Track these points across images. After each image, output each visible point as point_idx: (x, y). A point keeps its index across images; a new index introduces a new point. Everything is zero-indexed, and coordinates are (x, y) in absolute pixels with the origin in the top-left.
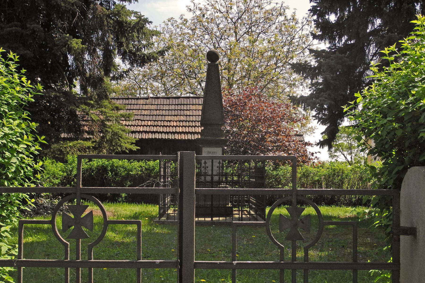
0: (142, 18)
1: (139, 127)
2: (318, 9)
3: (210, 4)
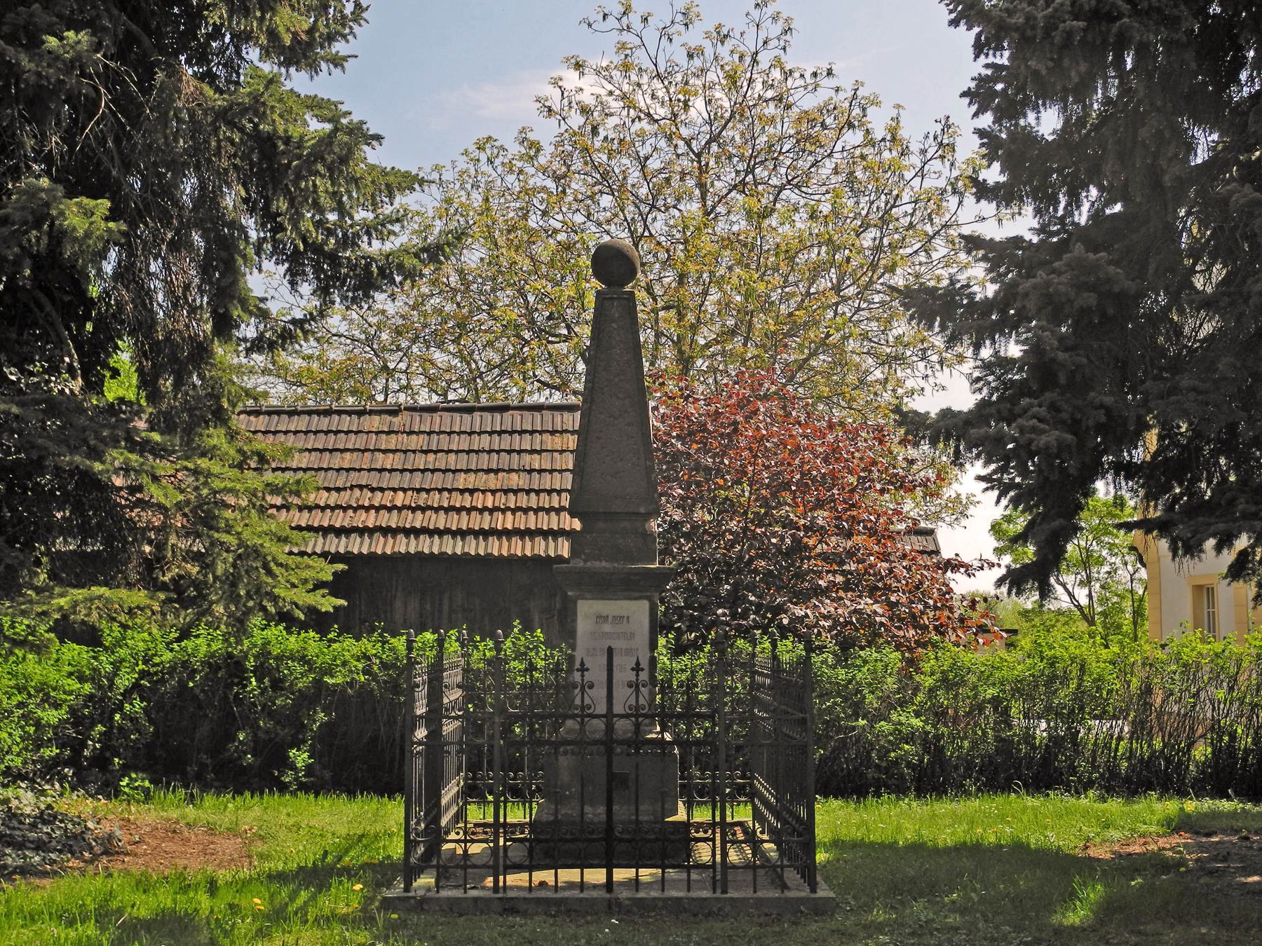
0: (344, 121)
1: (364, 515)
2: (999, 87)
3: (617, 92)
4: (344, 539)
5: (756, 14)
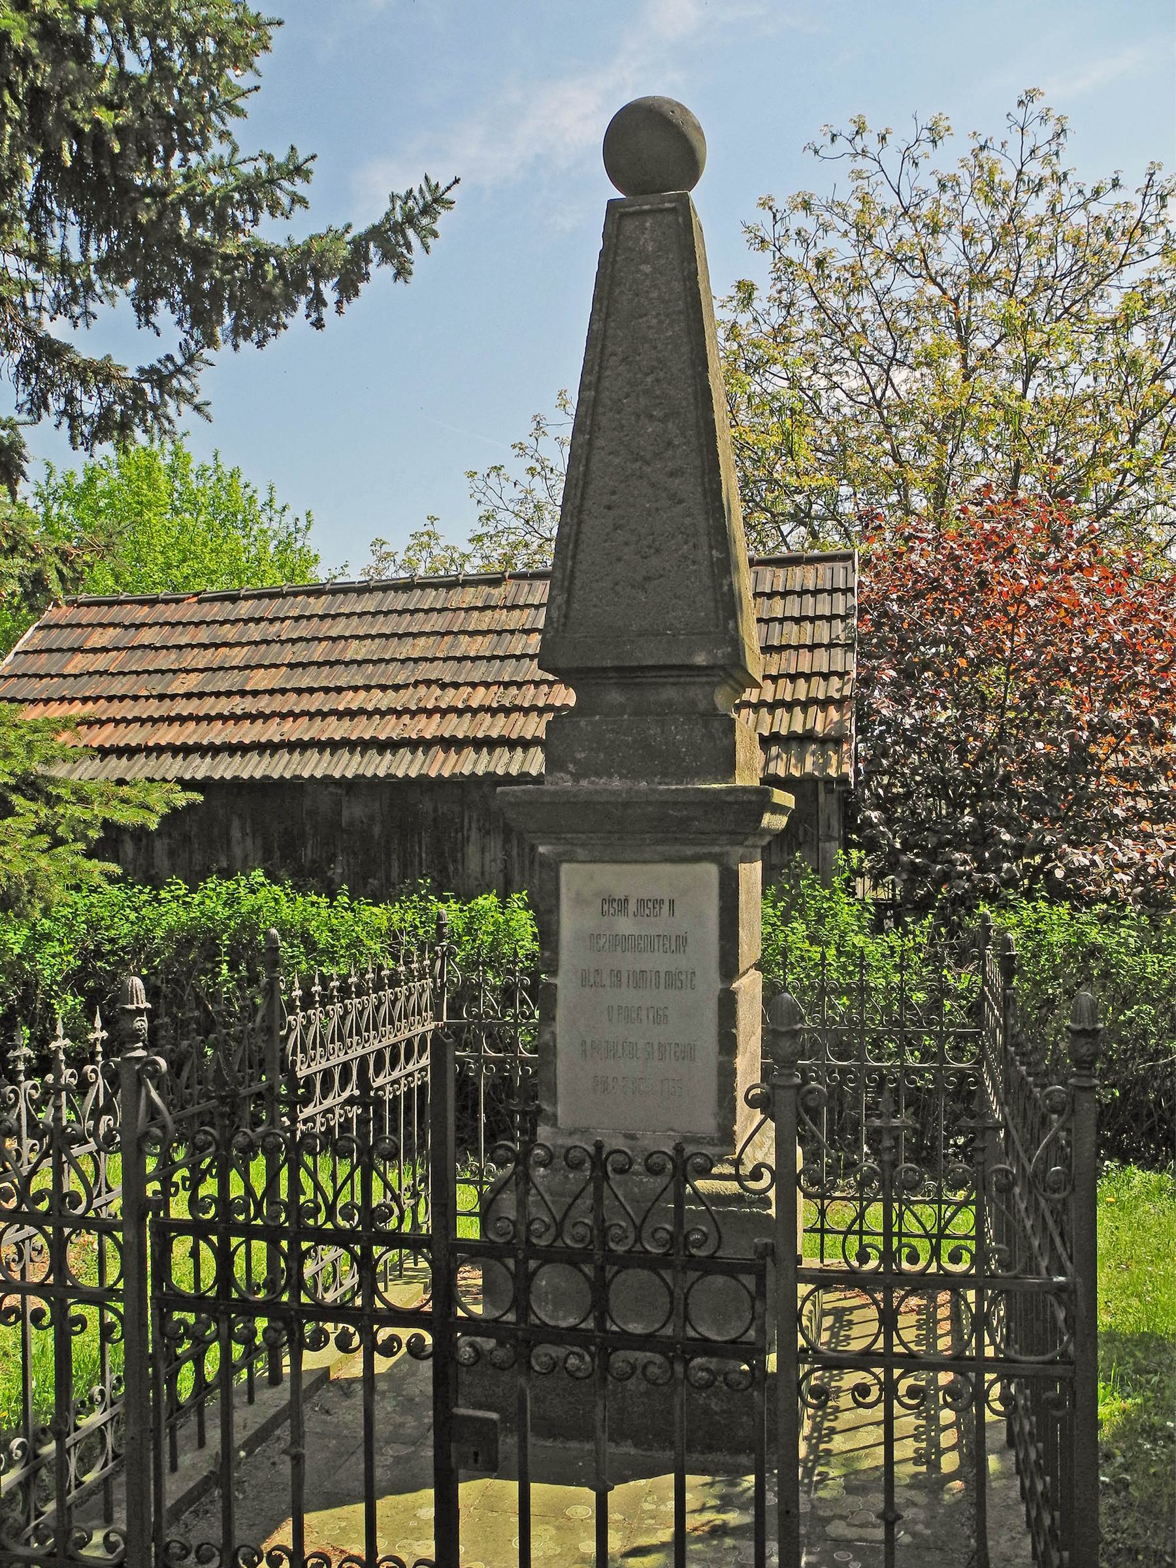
4: (357, 757)
5: (1019, 114)
